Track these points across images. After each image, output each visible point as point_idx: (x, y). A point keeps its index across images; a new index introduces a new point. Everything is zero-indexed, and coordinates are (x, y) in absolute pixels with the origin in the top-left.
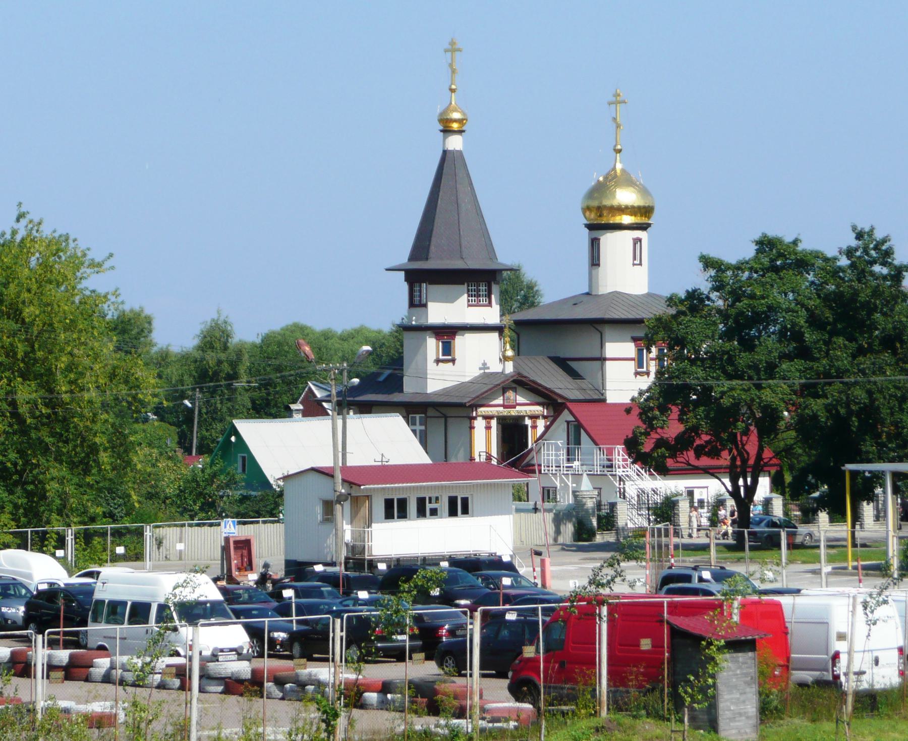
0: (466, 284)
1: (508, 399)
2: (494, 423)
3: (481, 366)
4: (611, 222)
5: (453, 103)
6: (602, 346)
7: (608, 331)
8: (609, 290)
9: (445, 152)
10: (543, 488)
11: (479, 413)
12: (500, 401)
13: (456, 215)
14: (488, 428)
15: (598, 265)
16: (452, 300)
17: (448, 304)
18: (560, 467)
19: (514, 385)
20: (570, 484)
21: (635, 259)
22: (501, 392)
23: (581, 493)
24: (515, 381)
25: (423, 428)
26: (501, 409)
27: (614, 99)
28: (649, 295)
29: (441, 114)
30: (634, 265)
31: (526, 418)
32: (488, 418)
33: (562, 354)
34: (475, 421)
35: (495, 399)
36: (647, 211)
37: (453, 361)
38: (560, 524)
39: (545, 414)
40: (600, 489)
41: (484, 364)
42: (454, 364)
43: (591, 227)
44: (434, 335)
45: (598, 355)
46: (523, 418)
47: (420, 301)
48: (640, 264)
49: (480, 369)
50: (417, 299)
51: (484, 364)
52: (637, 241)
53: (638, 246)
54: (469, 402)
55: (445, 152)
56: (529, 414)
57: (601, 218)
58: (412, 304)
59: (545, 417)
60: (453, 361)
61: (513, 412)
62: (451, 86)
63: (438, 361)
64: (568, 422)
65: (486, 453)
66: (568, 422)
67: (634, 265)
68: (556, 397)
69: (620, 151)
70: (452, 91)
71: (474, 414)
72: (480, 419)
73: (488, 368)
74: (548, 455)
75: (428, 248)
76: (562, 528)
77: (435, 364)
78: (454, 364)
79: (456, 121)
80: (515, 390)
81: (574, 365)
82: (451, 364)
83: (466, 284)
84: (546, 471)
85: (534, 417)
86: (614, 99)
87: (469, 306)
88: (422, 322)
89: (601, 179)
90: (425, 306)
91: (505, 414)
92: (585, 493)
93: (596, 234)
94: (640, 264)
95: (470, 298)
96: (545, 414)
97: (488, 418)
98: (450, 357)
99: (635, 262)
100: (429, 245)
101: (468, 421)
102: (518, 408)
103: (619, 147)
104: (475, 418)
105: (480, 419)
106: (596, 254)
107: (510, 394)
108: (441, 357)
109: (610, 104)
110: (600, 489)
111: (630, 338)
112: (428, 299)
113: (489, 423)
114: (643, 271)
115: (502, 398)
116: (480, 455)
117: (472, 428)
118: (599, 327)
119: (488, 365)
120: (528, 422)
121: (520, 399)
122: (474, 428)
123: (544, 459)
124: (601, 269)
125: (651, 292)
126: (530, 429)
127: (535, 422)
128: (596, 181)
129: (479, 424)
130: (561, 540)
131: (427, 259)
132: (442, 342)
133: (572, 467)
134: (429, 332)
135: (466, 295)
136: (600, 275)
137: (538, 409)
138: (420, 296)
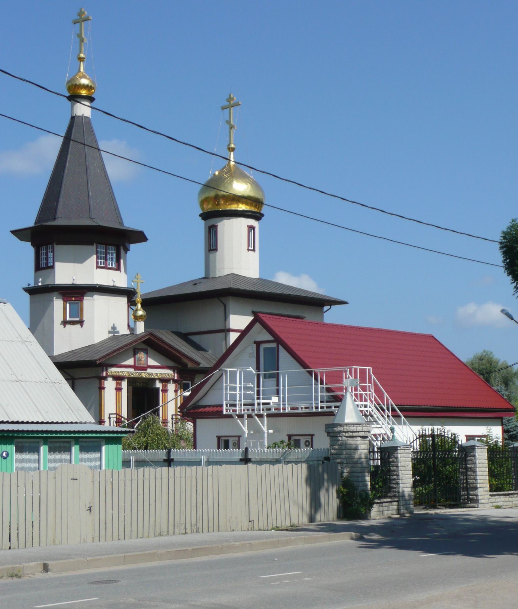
0: (95, 245)
1: (140, 360)
2: (124, 384)
3: (110, 330)
4: (228, 209)
5: (82, 70)
6: (226, 318)
7: (232, 303)
8: (227, 272)
9: (73, 118)
10: (219, 438)
11: (109, 373)
12: (130, 362)
13: (85, 177)
14: (118, 389)
15: (216, 250)
16: (81, 260)
17: (77, 265)
18: (253, 405)
19: (144, 346)
20: (265, 429)
21: (249, 246)
22: (132, 353)
23: (346, 429)
24: (145, 342)
25: (52, 250)
26: (132, 370)
27: (228, 103)
28: (259, 279)
29: (69, 82)
30: (249, 250)
31: (157, 382)
32: (118, 379)
33: (183, 331)
34: (106, 382)
35: (122, 363)
36: (257, 202)
37: (81, 322)
38: (319, 489)
39: (176, 378)
40: (312, 435)
41: (114, 328)
42: (82, 326)
43: (205, 216)
44: (61, 296)
45: (220, 327)
46: (153, 380)
47: (47, 263)
48: (254, 250)
49: (110, 332)
50: (43, 262)
51: (114, 328)
52: (251, 228)
53: (252, 234)
54: (100, 359)
55: (73, 118)
56: (160, 377)
57: (219, 206)
58: (38, 268)
59: (175, 381)
60: (81, 322)
61: (144, 374)
62: (79, 55)
63: (65, 323)
64: (258, 344)
65: (116, 414)
66: (258, 344)
67: (249, 250)
68: (185, 360)
69: (233, 150)
70: (81, 59)
71: (104, 374)
72: (110, 379)
73: (118, 332)
74: (234, 389)
75: (55, 209)
76: (322, 494)
77: (62, 326)
78: (82, 326)
79: (86, 87)
80: (146, 351)
81: (194, 338)
82: (78, 326)
83: (95, 245)
84: (231, 413)
85: (165, 381)
86: (228, 103)
87: (98, 267)
88: (48, 282)
89: (217, 173)
90: (52, 267)
91: (137, 375)
92: (353, 428)
93: (212, 222)
94: (254, 250)
95: (99, 260)
96: (176, 378)
97: (118, 379)
98: (78, 319)
99: (250, 248)
100: (57, 206)
101: (97, 381)
102: (149, 370)
103: (232, 146)
104: (105, 378)
105: (110, 379)
106: (213, 240)
107: (141, 356)
108: (68, 319)
109: (223, 108)
110: (312, 435)
111: (250, 311)
112: (56, 258)
113: (120, 384)
114: (255, 257)
115: (132, 359)
116: (110, 418)
117: (101, 388)
118: (223, 299)
119: (117, 330)
120: (159, 385)
121: (151, 362)
122: (104, 388)
123: (226, 394)
124: (218, 253)
125: (262, 277)
126: (161, 393)
127: (165, 386)
128: (212, 175)
129: (110, 385)
130: (321, 517)
131: (54, 219)
132: (69, 304)
133: (268, 404)
134: (56, 293)
135: (94, 257)
136: (217, 259)
137: (168, 373)
138: (47, 259)
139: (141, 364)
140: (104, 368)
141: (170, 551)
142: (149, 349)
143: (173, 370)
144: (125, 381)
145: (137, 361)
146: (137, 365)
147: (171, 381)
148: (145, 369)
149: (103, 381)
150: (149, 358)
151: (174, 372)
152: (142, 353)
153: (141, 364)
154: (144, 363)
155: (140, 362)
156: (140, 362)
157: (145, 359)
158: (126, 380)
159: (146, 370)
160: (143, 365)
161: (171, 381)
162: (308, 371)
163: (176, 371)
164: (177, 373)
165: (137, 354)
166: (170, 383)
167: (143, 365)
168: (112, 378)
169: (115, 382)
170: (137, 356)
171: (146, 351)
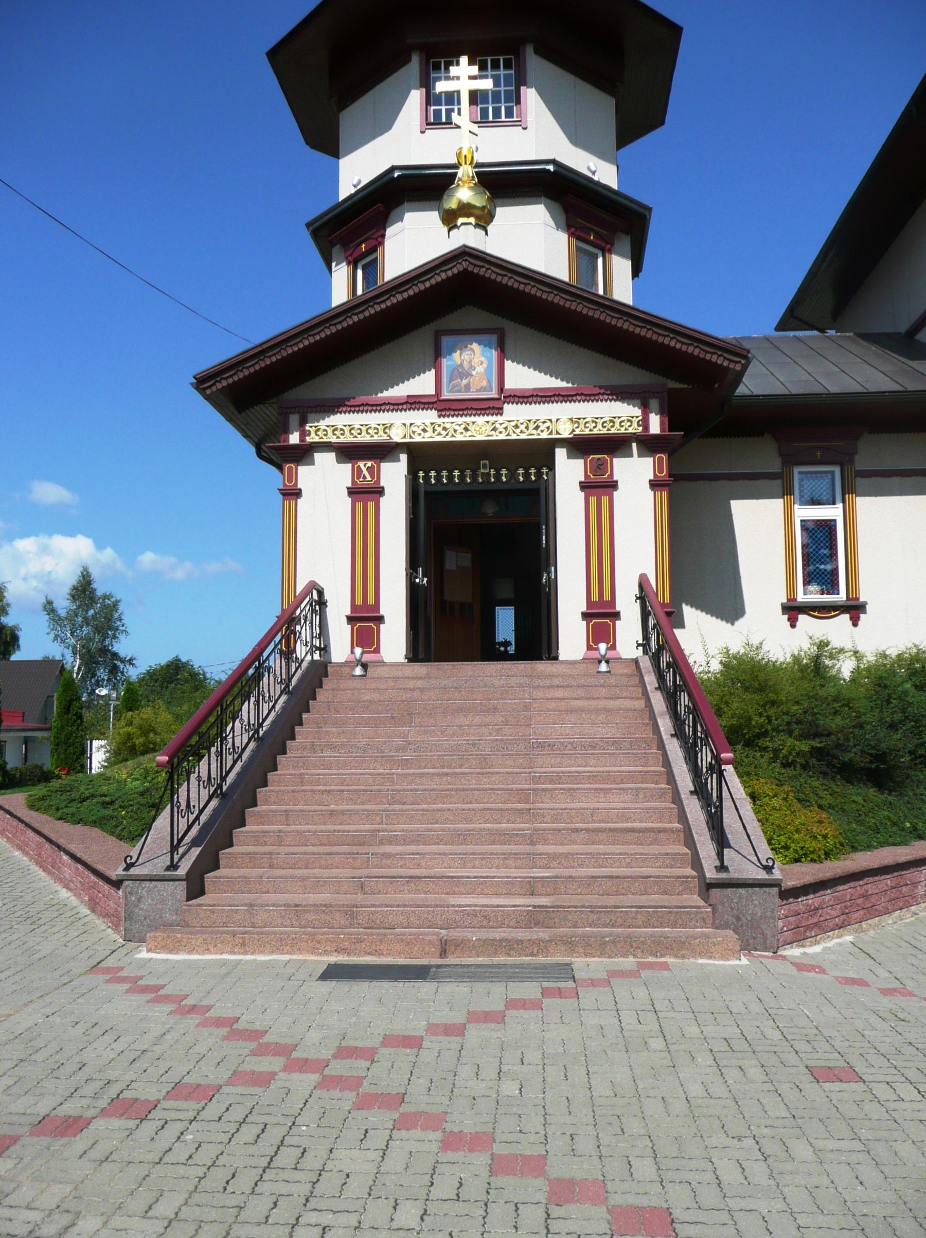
4: (346, 190)
26: (430, 416)
31: (561, 454)
59: (649, 444)
72: (325, 460)
102: (512, 411)
105: (325, 460)
115: (430, 375)
139: (467, 388)
140: (294, 419)
141: (526, 956)
142: (509, 326)
143: (638, 402)
144: (398, 460)
145: (451, 379)
146: (446, 395)
147: (634, 445)
148: (491, 407)
149: (661, 471)
150: (508, 364)
151: (646, 409)
152: (475, 346)
153: (467, 388)
154: (484, 383)
155: (464, 382)
156: (464, 382)
157: (488, 370)
158: (404, 457)
159: (499, 411)
160: (477, 391)
161: (634, 445)
162: (560, 434)
163: (654, 403)
164: (661, 413)
165: (451, 351)
166: (631, 455)
167: (477, 391)
168: (333, 454)
169: (581, 462)
170: (445, 362)
171: (494, 338)
